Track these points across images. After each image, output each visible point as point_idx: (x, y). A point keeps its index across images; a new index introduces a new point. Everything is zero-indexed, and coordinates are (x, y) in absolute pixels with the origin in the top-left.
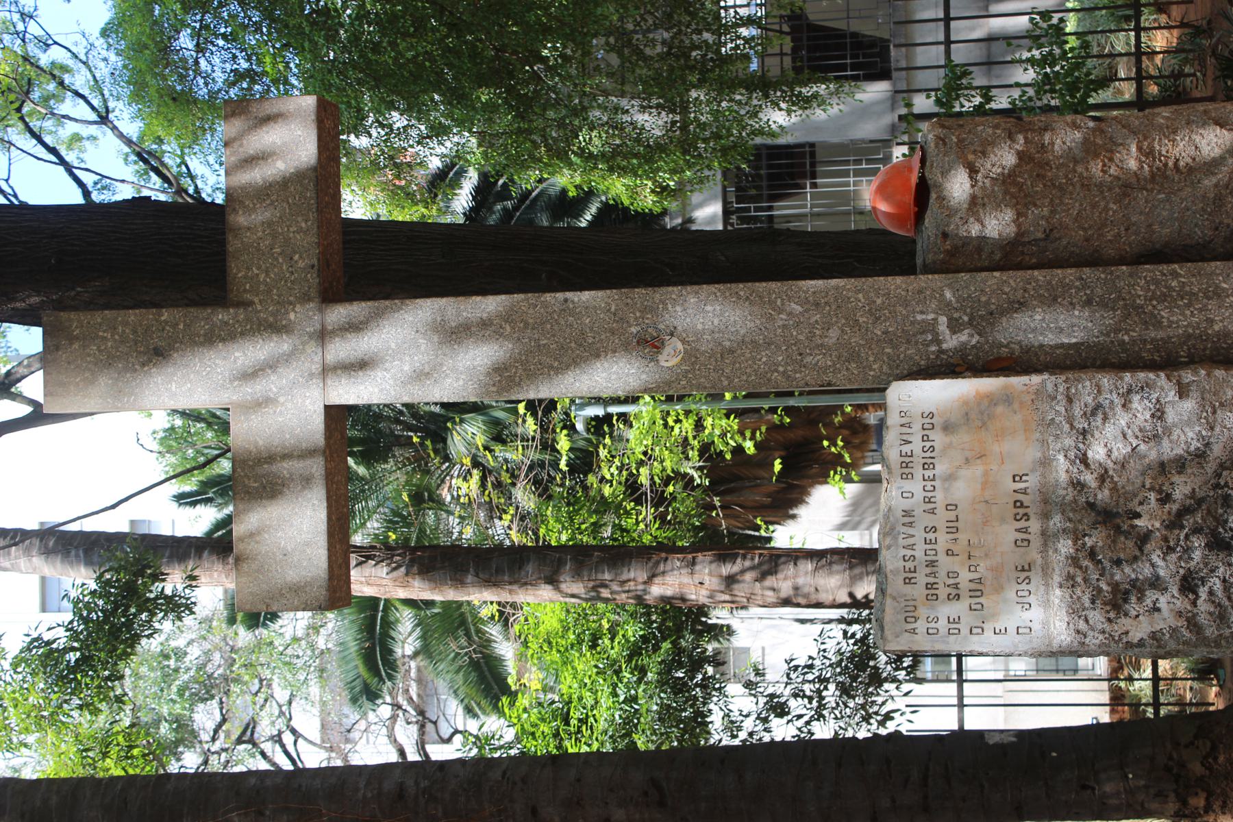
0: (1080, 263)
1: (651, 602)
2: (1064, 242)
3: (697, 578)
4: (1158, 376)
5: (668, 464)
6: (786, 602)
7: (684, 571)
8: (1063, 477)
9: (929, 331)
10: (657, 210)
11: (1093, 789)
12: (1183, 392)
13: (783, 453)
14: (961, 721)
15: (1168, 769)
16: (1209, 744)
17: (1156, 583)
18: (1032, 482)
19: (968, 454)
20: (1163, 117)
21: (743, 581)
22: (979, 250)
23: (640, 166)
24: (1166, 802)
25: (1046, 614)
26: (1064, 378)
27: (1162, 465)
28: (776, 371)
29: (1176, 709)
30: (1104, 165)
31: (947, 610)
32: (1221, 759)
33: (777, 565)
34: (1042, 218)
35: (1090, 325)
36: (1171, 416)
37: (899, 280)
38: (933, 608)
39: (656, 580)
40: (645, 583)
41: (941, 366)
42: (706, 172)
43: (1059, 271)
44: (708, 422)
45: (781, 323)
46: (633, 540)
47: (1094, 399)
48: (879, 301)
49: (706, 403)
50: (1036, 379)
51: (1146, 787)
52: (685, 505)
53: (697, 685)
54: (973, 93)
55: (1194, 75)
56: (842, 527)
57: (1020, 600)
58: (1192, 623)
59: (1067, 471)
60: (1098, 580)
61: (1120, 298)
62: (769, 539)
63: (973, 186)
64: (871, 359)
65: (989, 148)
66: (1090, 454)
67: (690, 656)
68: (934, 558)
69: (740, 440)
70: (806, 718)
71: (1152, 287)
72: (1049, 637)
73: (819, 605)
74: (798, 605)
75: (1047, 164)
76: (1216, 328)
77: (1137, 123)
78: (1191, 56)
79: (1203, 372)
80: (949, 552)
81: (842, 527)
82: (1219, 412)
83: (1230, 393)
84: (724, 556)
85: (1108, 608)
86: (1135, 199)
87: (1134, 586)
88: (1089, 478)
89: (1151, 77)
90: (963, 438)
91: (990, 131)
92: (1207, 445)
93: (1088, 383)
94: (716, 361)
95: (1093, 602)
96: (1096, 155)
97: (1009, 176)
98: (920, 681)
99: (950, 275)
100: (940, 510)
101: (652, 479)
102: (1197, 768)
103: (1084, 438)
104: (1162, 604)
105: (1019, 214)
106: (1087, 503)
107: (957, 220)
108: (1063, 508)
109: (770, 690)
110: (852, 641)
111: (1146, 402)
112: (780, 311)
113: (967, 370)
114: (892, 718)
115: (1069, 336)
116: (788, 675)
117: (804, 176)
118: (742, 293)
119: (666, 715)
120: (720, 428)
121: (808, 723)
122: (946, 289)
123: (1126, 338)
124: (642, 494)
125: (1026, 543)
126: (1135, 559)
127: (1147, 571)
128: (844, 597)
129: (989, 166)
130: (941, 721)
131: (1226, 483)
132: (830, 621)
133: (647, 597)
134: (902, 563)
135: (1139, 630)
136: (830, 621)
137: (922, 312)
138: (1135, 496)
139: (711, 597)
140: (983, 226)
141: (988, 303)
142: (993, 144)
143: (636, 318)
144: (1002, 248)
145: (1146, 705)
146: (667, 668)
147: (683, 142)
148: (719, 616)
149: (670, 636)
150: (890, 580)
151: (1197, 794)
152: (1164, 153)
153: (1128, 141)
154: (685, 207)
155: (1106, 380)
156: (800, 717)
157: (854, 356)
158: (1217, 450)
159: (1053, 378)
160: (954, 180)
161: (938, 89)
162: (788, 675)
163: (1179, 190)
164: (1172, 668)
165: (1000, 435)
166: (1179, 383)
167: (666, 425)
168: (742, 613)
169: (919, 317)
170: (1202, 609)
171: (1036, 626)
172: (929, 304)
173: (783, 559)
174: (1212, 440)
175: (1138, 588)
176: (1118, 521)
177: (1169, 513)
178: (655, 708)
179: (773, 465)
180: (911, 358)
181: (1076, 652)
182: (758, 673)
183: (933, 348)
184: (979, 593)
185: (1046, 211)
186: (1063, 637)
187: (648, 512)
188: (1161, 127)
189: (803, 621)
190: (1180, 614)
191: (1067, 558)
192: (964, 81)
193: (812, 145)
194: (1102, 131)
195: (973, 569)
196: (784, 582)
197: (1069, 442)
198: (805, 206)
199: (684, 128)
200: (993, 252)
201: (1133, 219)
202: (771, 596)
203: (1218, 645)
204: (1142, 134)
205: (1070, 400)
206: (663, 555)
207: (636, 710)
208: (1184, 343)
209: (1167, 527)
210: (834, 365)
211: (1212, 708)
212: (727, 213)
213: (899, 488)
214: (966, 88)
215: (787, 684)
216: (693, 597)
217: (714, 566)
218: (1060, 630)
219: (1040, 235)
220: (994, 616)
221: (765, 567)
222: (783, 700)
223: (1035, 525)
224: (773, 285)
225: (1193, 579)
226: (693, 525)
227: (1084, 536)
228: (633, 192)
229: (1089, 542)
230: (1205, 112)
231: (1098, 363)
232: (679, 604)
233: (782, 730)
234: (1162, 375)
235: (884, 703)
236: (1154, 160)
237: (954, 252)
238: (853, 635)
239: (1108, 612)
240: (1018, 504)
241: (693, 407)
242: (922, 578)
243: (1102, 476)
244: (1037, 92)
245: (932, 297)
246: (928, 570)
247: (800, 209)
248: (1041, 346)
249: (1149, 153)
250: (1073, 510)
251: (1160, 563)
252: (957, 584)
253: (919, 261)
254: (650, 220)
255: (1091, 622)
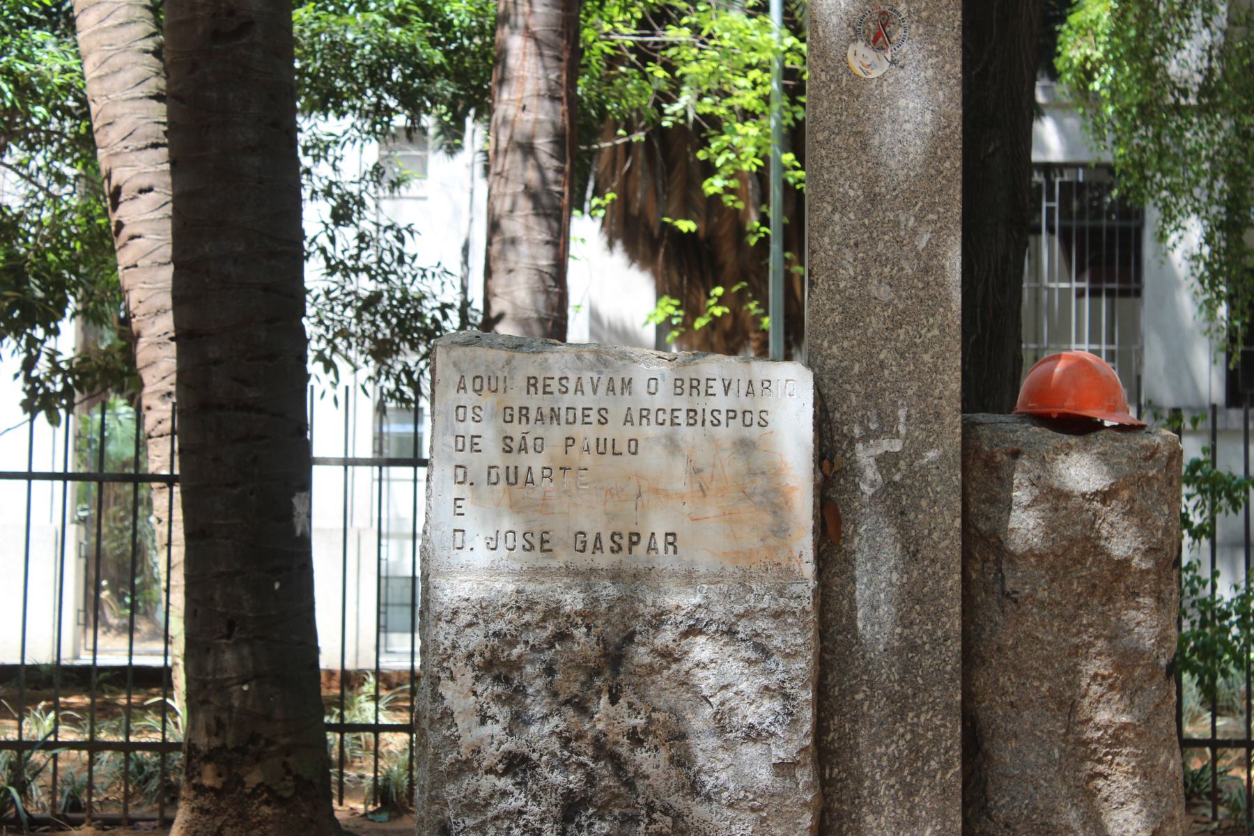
0: (966, 636)
1: (499, 35)
2: (997, 619)
3: (532, 102)
4: (806, 736)
5: (694, 68)
6: (494, 227)
7: (542, 84)
8: (670, 601)
9: (882, 425)
10: (1059, 64)
11: (229, 637)
12: (783, 769)
13: (702, 234)
14: (325, 461)
15: (254, 738)
16: (287, 794)
17: (519, 721)
18: (665, 560)
19: (707, 474)
20: (1167, 761)
21: (525, 168)
22: (993, 501)
23: (1125, 40)
24: (209, 733)
25: (481, 567)
26: (809, 607)
27: (683, 736)
28: (834, 210)
29: (335, 756)
30: (1104, 677)
31: (489, 433)
32: (266, 810)
33: (547, 216)
34: (1035, 590)
35: (881, 647)
36: (751, 751)
37: (956, 386)
38: (494, 415)
39: (531, 45)
40: (527, 27)
41: (832, 441)
42: (1110, 137)
43: (958, 609)
44: (751, 129)
45: (902, 218)
46: (588, 15)
47: (778, 649)
48: (927, 358)
49: (779, 125)
50: (809, 570)
51: (230, 708)
52: (634, 93)
53: (380, 98)
54: (1207, 513)
55: (1215, 818)
56: (595, 317)
57: (502, 535)
58: (463, 767)
59: (678, 607)
60: (527, 643)
61: (917, 689)
62: (581, 209)
63: (1083, 495)
64: (846, 344)
65: (1136, 520)
66: (701, 639)
67: (420, 91)
68: (563, 420)
69: (723, 173)
70: (329, 248)
71: (930, 734)
72: (450, 573)
73: (488, 273)
74: (489, 243)
75: (1110, 600)
76: (870, 818)
77: (1162, 725)
78: (1241, 815)
79: (809, 797)
80: (570, 441)
81: (595, 317)
82: (754, 816)
83: (779, 832)
84: (560, 141)
85: (487, 655)
86: (1054, 717)
87: (516, 690)
88: (667, 637)
89: (1215, 760)
90: (731, 465)
91: (1161, 523)
92: (708, 798)
93: (800, 640)
94: (852, 125)
95: (495, 634)
96: (1118, 667)
97: (1096, 547)
98: (381, 409)
99: (959, 459)
100: (630, 432)
101: (673, 45)
102: (253, 778)
103: (723, 633)
104: (490, 728)
105: (1041, 557)
106: (634, 633)
107: (1037, 472)
108: (629, 600)
109: (369, 202)
110: (439, 316)
111: (771, 718)
112: (919, 218)
113: (825, 476)
114: (327, 371)
115: (867, 618)
116: (391, 227)
117: (1093, 280)
118: (947, 164)
119: (340, 52)
120: (743, 145)
121: (323, 250)
122: (940, 453)
123: (860, 696)
124: (652, 29)
125: (580, 546)
126: (555, 694)
127: (537, 710)
128: (497, 307)
129: (1111, 518)
130: (325, 434)
131: (655, 821)
132: (464, 290)
133: (507, 29)
134: (557, 376)
135: (458, 694)
136: (464, 290)
137: (908, 417)
138: (642, 698)
139: (505, 121)
140: (1027, 507)
141: (917, 508)
142: (1142, 526)
143: (918, 11)
144: (994, 533)
145: (341, 716)
146: (406, 56)
147: (1152, 106)
148: (475, 133)
149: (451, 60)
150: (534, 357)
151: (219, 775)
152: (1117, 759)
153: (1136, 712)
154: (1058, 107)
155: (802, 666)
156: (332, 240)
157: (851, 321)
158: (700, 811)
159: (809, 593)
160: (1093, 470)
161: (1214, 466)
162: (391, 227)
163: (1064, 777)
164: (390, 752)
165: (729, 516)
166: (795, 764)
167: (750, 67)
168: (479, 169)
169: (902, 413)
170: (483, 781)
171: (464, 556)
172: (921, 431)
173: (555, 225)
174: (715, 805)
175: (514, 696)
176: (607, 674)
177: (616, 743)
178: (350, 36)
179: (686, 218)
180: (844, 399)
181: (428, 609)
182: (395, 185)
183: (857, 431)
184: (512, 479)
185: (1042, 594)
186: (448, 592)
187: (627, 37)
188: (1154, 757)
189: (466, 250)
190: (477, 751)
191: (559, 602)
192: (1224, 502)
193: (1138, 293)
194: (1152, 677)
195: (547, 472)
196: (524, 225)
197: (719, 611)
198: (1051, 279)
199: (1177, 108)
200: (988, 519)
201: (1026, 714)
202: (503, 205)
203: (433, 800)
204: (1142, 731)
205: (777, 615)
206: (566, 55)
207: (346, 10)
208: (850, 774)
209: (596, 739)
210: (840, 292)
211: (335, 803)
212: (1048, 168)
213: (663, 375)
214: (1213, 505)
215: (378, 225)
216: (505, 96)
217: (549, 127)
218: (455, 590)
219: (1009, 585)
220: (477, 499)
221: (545, 200)
222: (355, 217)
223: (604, 560)
224: (957, 210)
225: (524, 771)
226: (607, 102)
227: (588, 627)
228: (1087, 30)
229: (580, 633)
230: (1172, 818)
231: (827, 657)
232: (496, 75)
233: (315, 216)
234: (808, 742)
235: (348, 359)
236: (1107, 746)
237: (990, 465)
238: (445, 317)
239: (482, 654)
240: (634, 539)
241: (775, 106)
242: (534, 402)
243: (670, 654)
244: (1203, 602)
245: (930, 432)
246: (546, 411)
247: (1049, 271)
248: (854, 580)
249: (1117, 738)
250: (623, 614)
251: (547, 728)
252: (526, 450)
253: (980, 417)
254: (1044, 55)
255: (468, 630)
